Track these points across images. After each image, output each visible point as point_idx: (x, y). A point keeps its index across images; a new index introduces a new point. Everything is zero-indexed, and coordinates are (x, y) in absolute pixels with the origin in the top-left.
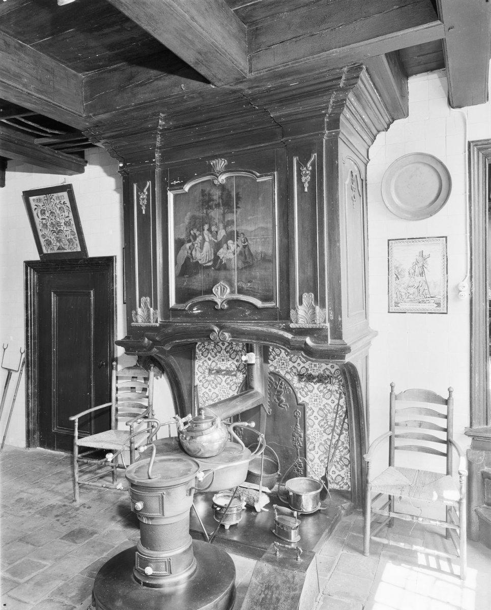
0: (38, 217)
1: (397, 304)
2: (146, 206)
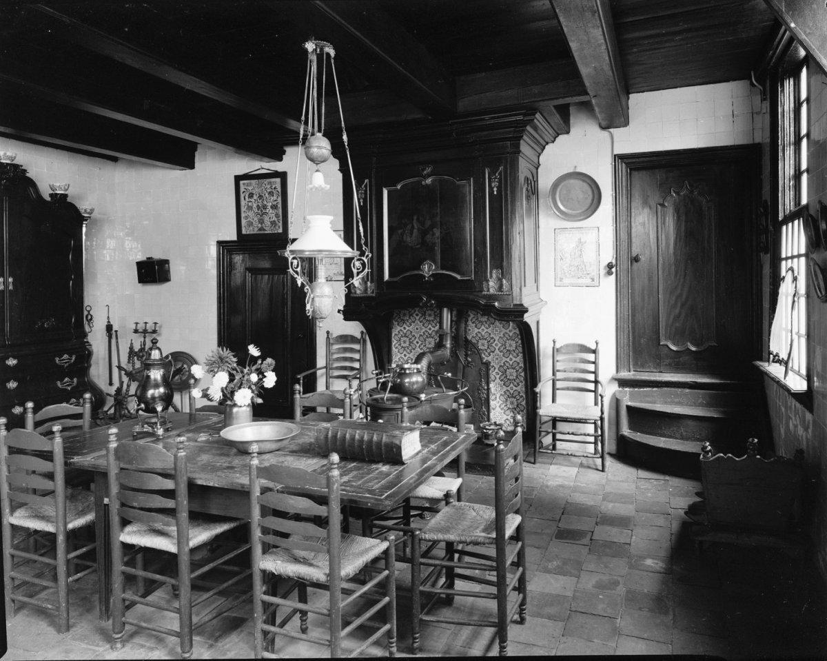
0: (245, 199)
1: (561, 279)
2: (364, 199)
